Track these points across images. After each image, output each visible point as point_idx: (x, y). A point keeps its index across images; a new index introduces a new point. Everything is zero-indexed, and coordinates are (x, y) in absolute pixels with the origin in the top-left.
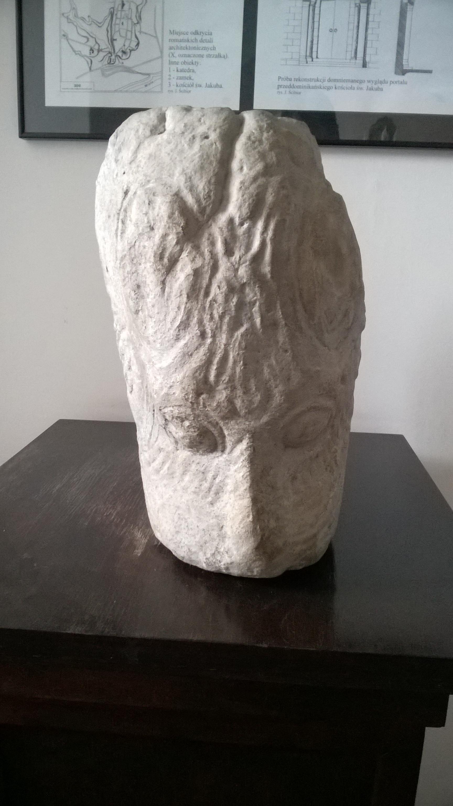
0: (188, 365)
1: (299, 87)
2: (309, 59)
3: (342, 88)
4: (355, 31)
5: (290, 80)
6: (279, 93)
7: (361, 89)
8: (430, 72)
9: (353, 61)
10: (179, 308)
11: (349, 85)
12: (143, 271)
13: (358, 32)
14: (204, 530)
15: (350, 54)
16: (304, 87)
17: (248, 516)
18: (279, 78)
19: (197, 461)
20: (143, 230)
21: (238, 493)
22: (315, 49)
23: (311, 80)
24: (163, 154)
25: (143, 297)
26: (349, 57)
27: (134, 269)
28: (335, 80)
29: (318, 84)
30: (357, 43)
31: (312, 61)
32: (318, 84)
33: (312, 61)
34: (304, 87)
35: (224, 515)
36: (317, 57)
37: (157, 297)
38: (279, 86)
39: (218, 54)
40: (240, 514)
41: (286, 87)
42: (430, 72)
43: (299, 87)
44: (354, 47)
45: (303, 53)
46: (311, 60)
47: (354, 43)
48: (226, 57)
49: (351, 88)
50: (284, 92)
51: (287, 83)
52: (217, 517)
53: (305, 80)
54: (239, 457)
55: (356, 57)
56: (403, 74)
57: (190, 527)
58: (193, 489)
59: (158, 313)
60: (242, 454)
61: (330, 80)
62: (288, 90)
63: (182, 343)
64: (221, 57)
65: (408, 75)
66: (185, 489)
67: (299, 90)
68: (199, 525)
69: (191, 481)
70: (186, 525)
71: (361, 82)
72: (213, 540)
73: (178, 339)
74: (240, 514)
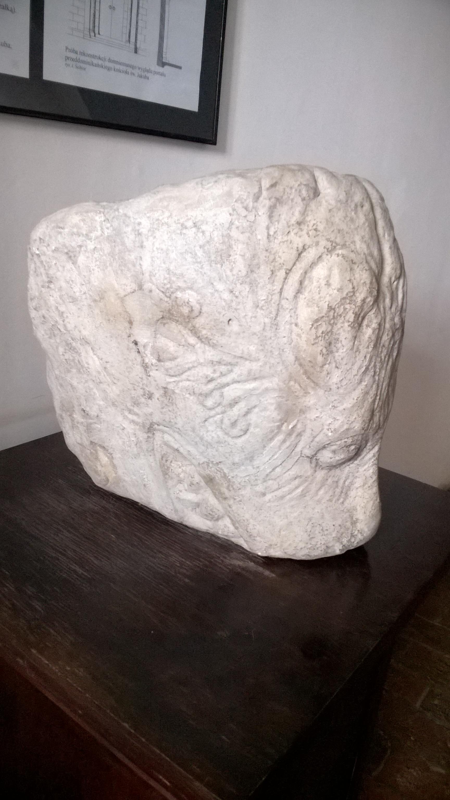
0: (366, 402)
1: (83, 62)
2: (92, 34)
3: (119, 71)
4: (129, 13)
5: (76, 53)
6: (67, 65)
7: (134, 74)
8: (180, 68)
9: (128, 44)
10: (365, 357)
11: (124, 68)
12: (338, 329)
13: (131, 15)
14: (340, 525)
15: (126, 37)
16: (88, 63)
17: (377, 500)
18: (67, 48)
19: (333, 475)
20: (347, 294)
21: (366, 486)
22: (97, 24)
23: (94, 57)
24: (337, 220)
25: (332, 352)
26: (124, 40)
27: (329, 329)
28: (114, 62)
29: (100, 62)
30: (130, 27)
31: (95, 36)
32: (100, 62)
33: (95, 36)
34: (88, 63)
35: (354, 507)
36: (99, 34)
37: (348, 351)
38: (67, 58)
39: (4, 5)
40: (371, 500)
41: (72, 60)
42: (180, 68)
43: (83, 62)
44: (128, 31)
45: (87, 26)
46: (93, 34)
47: (128, 26)
48: (13, 10)
49: (126, 72)
50: (71, 66)
51: (73, 55)
52: (348, 511)
53: (89, 55)
54: (370, 459)
55: (129, 41)
56: (163, 66)
57: (325, 528)
58: (328, 498)
59: (346, 364)
60: (374, 456)
61: (110, 61)
62: (74, 63)
63: (364, 384)
64: (8, 9)
65: (166, 67)
66: (319, 501)
67: (83, 65)
68: (334, 524)
69: (326, 493)
70: (321, 528)
71: (133, 67)
72: (348, 529)
73: (361, 381)
74: (371, 500)
